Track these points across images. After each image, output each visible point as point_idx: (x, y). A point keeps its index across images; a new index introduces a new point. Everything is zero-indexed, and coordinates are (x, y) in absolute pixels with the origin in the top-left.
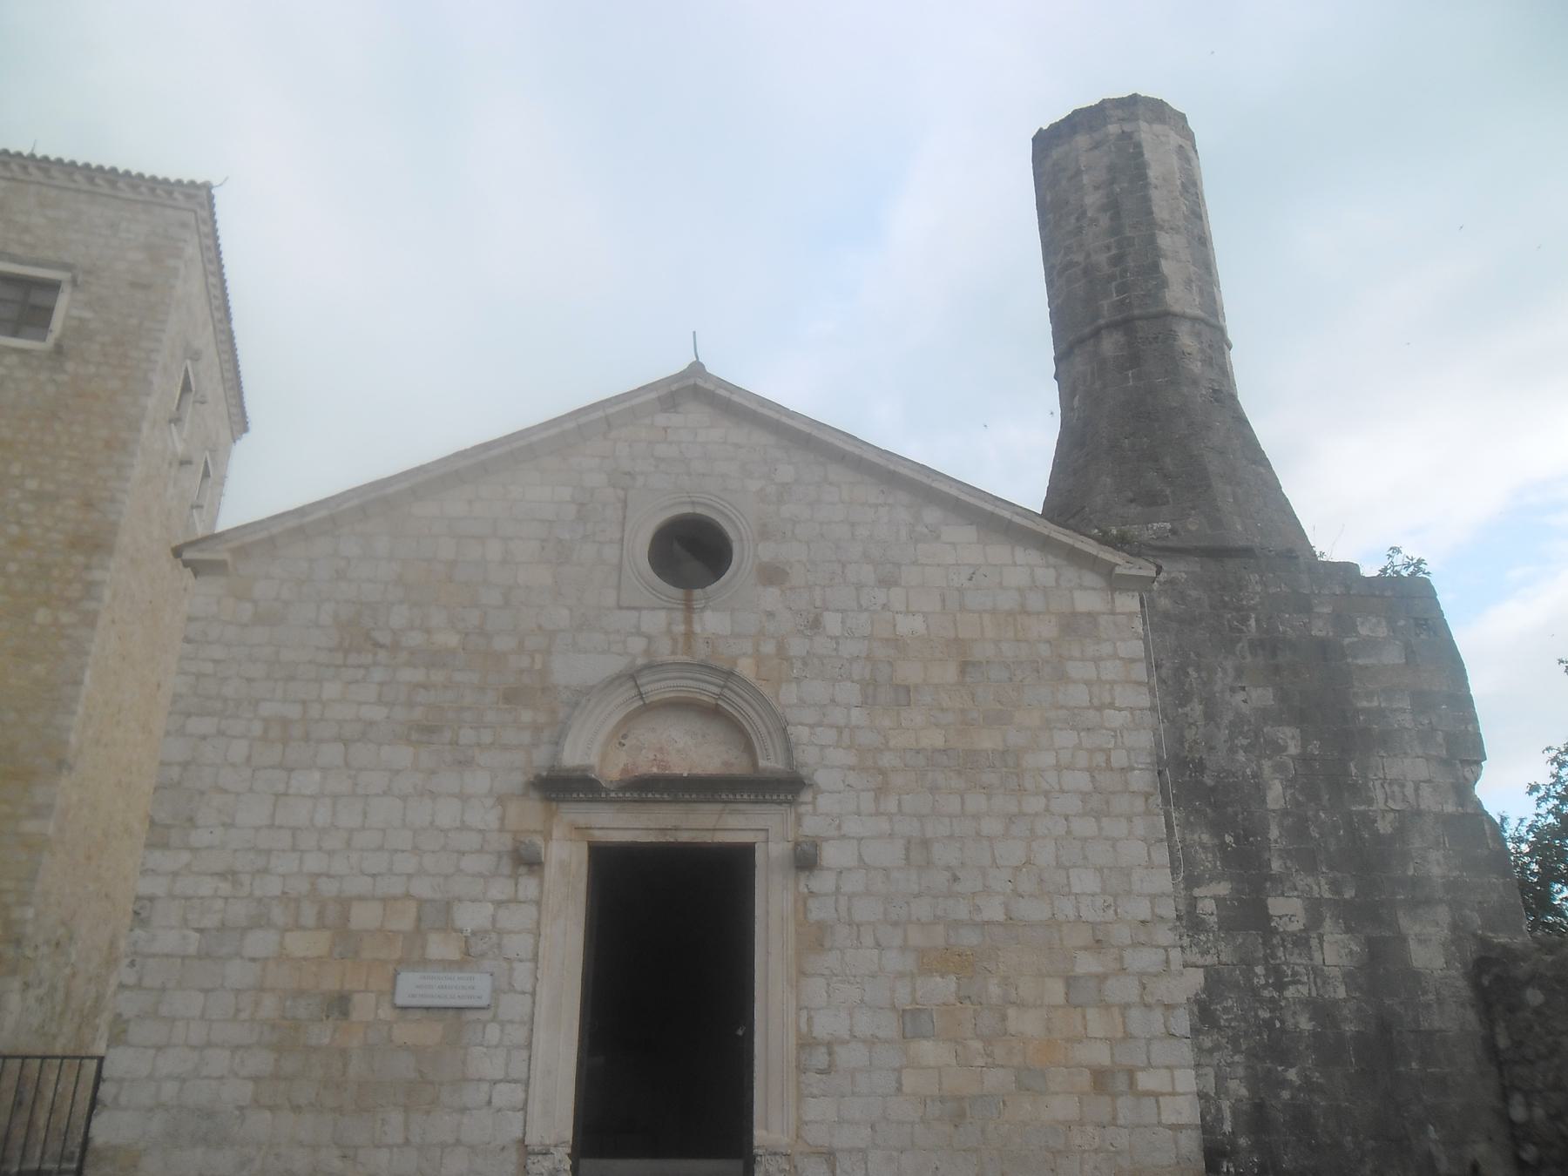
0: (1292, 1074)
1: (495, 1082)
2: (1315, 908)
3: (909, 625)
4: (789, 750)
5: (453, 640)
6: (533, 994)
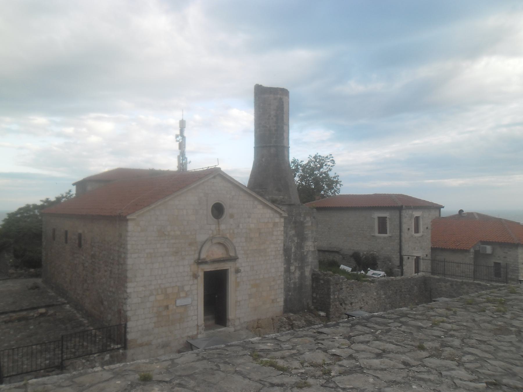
0: (290, 294)
1: (192, 316)
2: (296, 267)
3: (252, 226)
4: (236, 252)
5: (178, 233)
6: (197, 300)
